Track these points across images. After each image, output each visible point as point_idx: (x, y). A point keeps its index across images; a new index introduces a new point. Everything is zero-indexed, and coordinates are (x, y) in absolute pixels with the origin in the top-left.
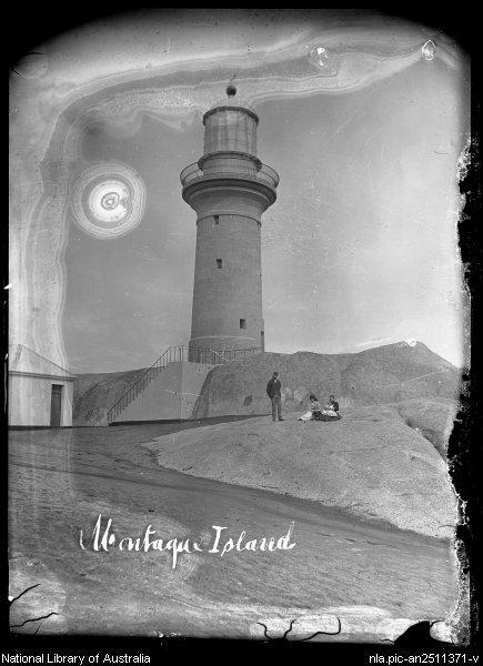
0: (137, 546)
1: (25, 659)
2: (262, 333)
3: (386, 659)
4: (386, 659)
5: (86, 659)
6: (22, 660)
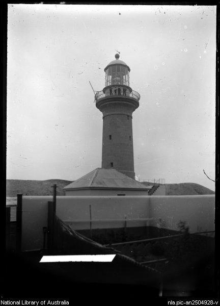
1: (11, 303)
3: (176, 303)
4: (176, 303)
5: (40, 303)
6: (10, 303)
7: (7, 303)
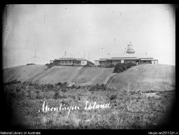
0: (57, 110)
1: (7, 133)
2: (28, 64)
3: (153, 133)
4: (153, 133)
5: (23, 133)
6: (6, 133)
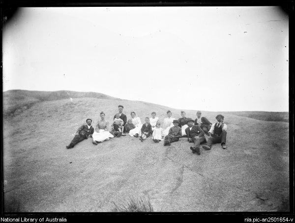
1: (11, 220)
3: (252, 220)
4: (252, 220)
5: (38, 220)
6: (10, 220)
7: (7, 220)
